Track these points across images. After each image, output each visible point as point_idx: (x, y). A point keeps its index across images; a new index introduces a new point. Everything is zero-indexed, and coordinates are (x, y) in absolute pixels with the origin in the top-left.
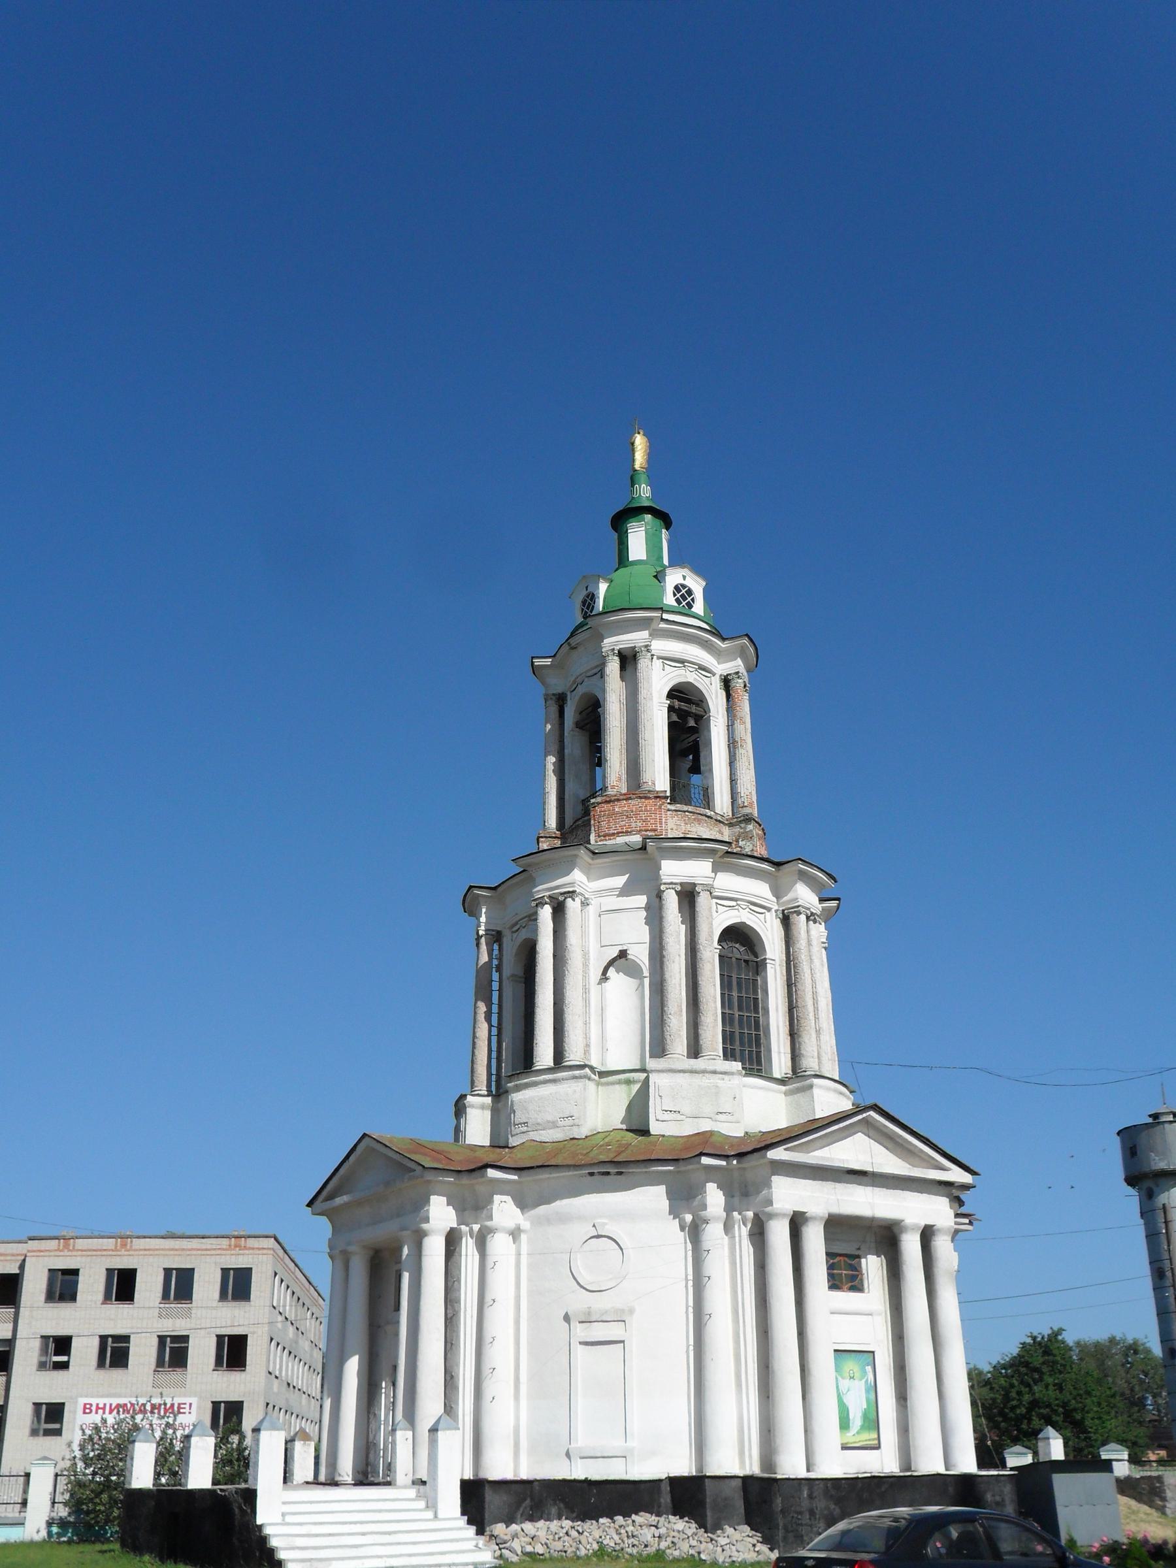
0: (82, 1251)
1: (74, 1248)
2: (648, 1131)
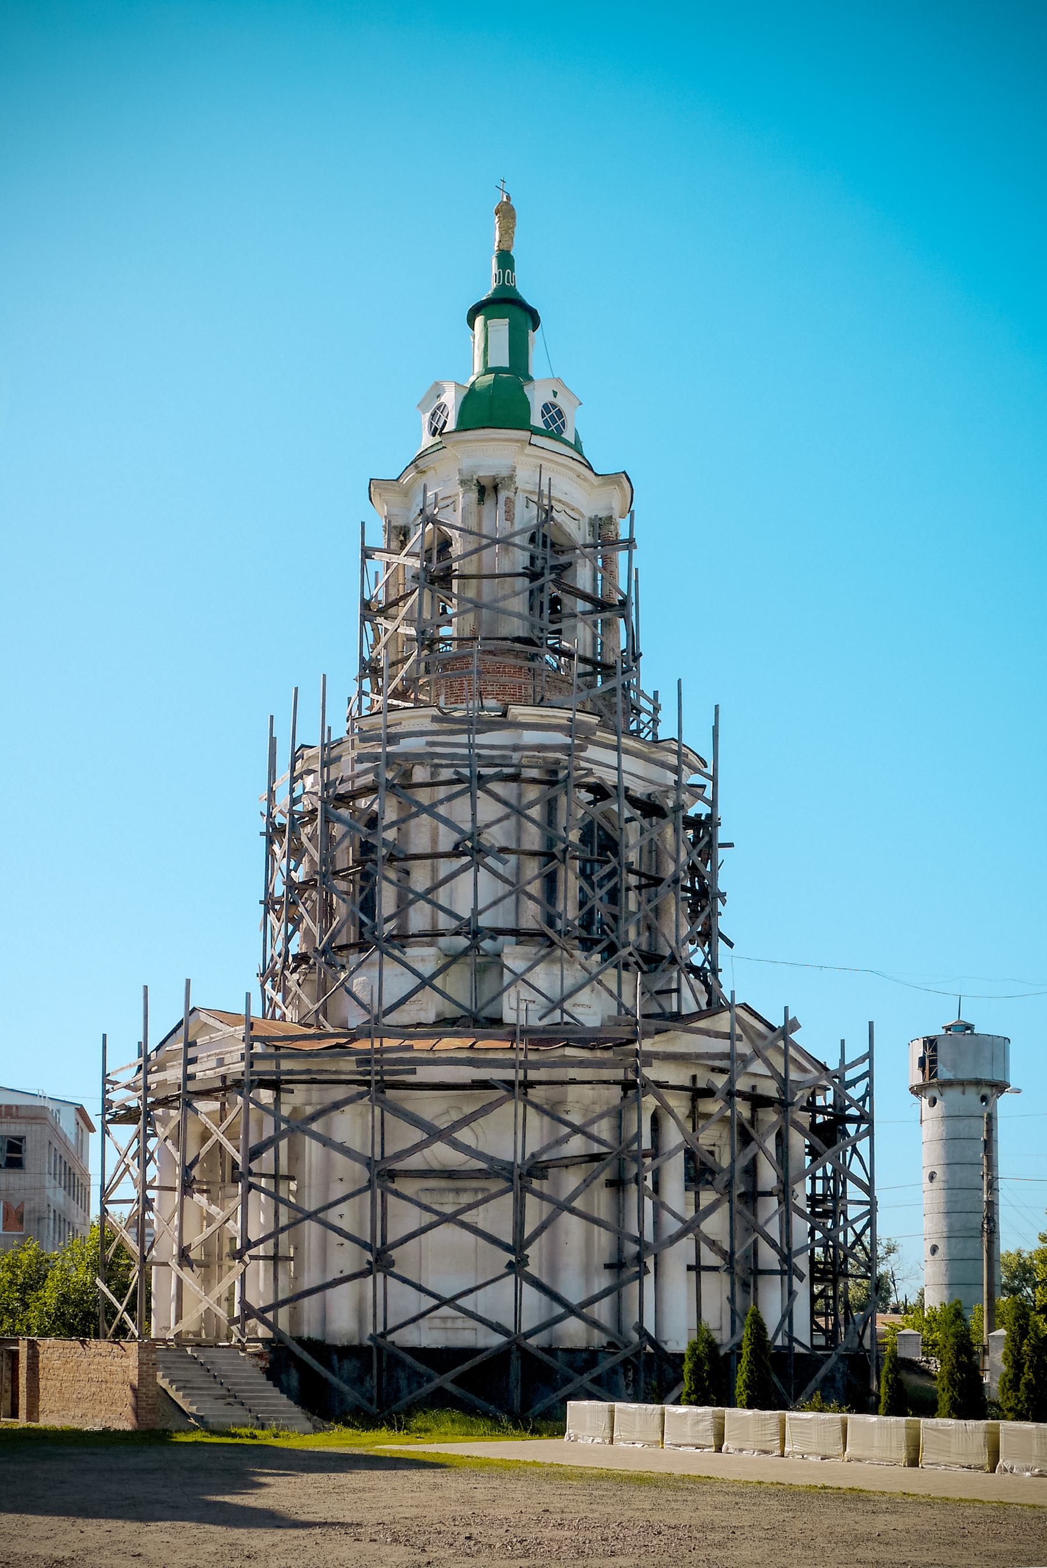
2: (501, 1020)
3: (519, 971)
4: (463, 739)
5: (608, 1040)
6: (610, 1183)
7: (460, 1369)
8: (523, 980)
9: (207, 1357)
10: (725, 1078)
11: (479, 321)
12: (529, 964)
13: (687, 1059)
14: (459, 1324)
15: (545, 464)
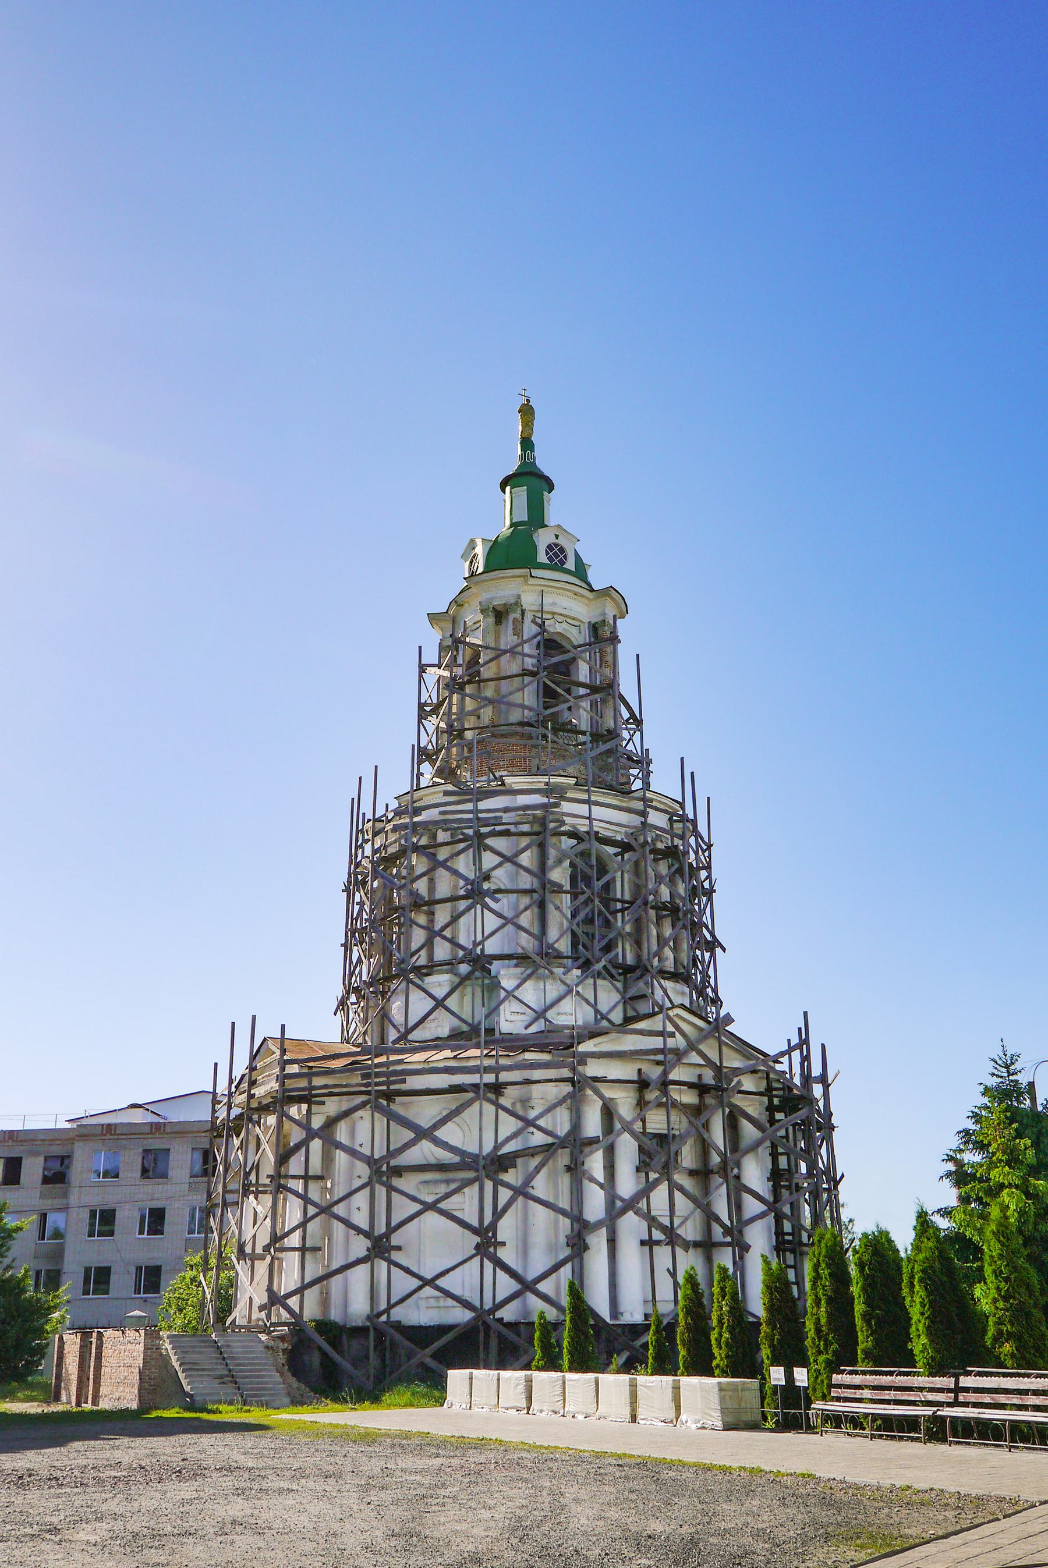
3: (509, 989)
4: (469, 806)
5: (550, 1044)
6: (569, 1169)
7: (437, 1345)
8: (515, 997)
9: (227, 1341)
10: (659, 1069)
11: (508, 489)
12: (519, 981)
13: (625, 1056)
14: (442, 1303)
15: (545, 589)
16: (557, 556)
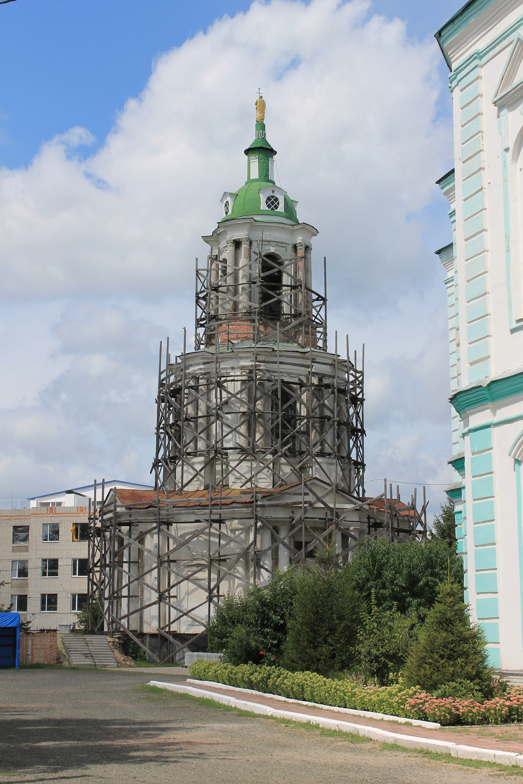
0: (59, 514)
1: (55, 512)
16: (273, 203)
